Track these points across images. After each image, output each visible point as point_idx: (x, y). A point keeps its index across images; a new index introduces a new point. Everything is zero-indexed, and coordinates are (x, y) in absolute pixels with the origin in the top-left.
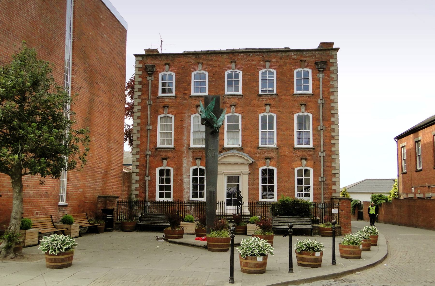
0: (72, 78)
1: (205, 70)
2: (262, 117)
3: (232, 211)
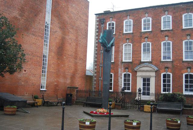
0: (51, 27)
1: (131, 19)
2: (163, 43)
3: (148, 98)
